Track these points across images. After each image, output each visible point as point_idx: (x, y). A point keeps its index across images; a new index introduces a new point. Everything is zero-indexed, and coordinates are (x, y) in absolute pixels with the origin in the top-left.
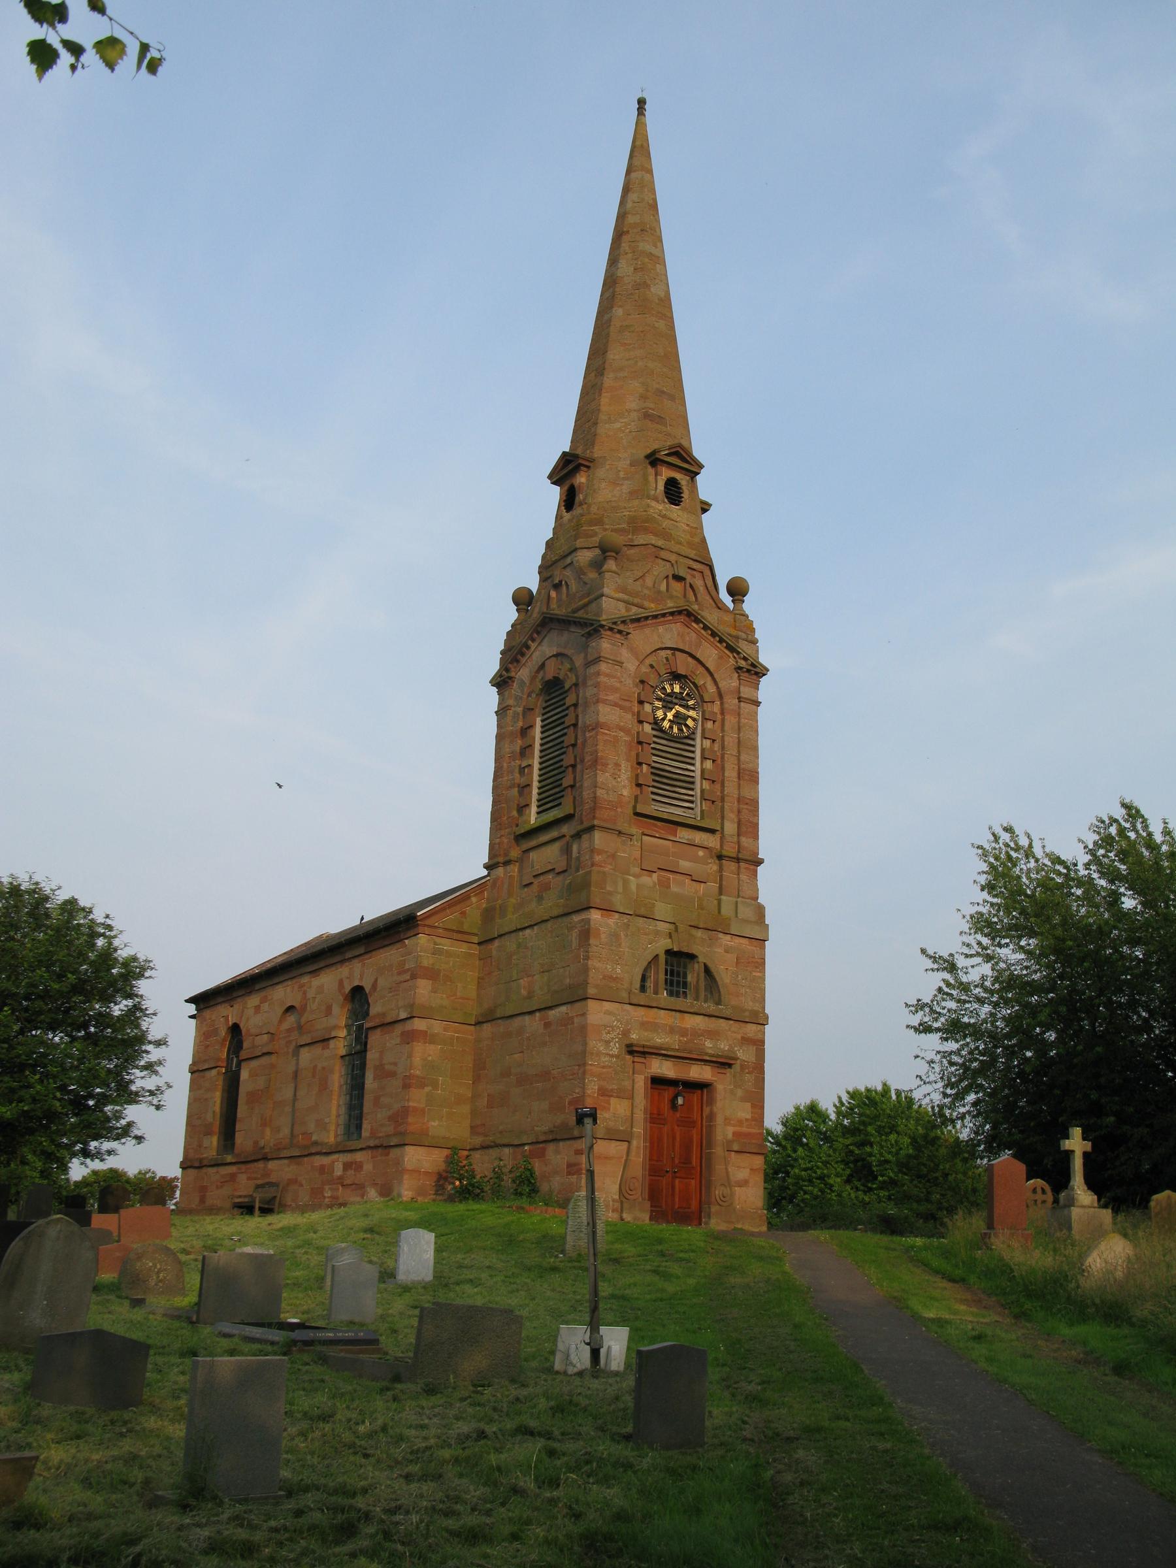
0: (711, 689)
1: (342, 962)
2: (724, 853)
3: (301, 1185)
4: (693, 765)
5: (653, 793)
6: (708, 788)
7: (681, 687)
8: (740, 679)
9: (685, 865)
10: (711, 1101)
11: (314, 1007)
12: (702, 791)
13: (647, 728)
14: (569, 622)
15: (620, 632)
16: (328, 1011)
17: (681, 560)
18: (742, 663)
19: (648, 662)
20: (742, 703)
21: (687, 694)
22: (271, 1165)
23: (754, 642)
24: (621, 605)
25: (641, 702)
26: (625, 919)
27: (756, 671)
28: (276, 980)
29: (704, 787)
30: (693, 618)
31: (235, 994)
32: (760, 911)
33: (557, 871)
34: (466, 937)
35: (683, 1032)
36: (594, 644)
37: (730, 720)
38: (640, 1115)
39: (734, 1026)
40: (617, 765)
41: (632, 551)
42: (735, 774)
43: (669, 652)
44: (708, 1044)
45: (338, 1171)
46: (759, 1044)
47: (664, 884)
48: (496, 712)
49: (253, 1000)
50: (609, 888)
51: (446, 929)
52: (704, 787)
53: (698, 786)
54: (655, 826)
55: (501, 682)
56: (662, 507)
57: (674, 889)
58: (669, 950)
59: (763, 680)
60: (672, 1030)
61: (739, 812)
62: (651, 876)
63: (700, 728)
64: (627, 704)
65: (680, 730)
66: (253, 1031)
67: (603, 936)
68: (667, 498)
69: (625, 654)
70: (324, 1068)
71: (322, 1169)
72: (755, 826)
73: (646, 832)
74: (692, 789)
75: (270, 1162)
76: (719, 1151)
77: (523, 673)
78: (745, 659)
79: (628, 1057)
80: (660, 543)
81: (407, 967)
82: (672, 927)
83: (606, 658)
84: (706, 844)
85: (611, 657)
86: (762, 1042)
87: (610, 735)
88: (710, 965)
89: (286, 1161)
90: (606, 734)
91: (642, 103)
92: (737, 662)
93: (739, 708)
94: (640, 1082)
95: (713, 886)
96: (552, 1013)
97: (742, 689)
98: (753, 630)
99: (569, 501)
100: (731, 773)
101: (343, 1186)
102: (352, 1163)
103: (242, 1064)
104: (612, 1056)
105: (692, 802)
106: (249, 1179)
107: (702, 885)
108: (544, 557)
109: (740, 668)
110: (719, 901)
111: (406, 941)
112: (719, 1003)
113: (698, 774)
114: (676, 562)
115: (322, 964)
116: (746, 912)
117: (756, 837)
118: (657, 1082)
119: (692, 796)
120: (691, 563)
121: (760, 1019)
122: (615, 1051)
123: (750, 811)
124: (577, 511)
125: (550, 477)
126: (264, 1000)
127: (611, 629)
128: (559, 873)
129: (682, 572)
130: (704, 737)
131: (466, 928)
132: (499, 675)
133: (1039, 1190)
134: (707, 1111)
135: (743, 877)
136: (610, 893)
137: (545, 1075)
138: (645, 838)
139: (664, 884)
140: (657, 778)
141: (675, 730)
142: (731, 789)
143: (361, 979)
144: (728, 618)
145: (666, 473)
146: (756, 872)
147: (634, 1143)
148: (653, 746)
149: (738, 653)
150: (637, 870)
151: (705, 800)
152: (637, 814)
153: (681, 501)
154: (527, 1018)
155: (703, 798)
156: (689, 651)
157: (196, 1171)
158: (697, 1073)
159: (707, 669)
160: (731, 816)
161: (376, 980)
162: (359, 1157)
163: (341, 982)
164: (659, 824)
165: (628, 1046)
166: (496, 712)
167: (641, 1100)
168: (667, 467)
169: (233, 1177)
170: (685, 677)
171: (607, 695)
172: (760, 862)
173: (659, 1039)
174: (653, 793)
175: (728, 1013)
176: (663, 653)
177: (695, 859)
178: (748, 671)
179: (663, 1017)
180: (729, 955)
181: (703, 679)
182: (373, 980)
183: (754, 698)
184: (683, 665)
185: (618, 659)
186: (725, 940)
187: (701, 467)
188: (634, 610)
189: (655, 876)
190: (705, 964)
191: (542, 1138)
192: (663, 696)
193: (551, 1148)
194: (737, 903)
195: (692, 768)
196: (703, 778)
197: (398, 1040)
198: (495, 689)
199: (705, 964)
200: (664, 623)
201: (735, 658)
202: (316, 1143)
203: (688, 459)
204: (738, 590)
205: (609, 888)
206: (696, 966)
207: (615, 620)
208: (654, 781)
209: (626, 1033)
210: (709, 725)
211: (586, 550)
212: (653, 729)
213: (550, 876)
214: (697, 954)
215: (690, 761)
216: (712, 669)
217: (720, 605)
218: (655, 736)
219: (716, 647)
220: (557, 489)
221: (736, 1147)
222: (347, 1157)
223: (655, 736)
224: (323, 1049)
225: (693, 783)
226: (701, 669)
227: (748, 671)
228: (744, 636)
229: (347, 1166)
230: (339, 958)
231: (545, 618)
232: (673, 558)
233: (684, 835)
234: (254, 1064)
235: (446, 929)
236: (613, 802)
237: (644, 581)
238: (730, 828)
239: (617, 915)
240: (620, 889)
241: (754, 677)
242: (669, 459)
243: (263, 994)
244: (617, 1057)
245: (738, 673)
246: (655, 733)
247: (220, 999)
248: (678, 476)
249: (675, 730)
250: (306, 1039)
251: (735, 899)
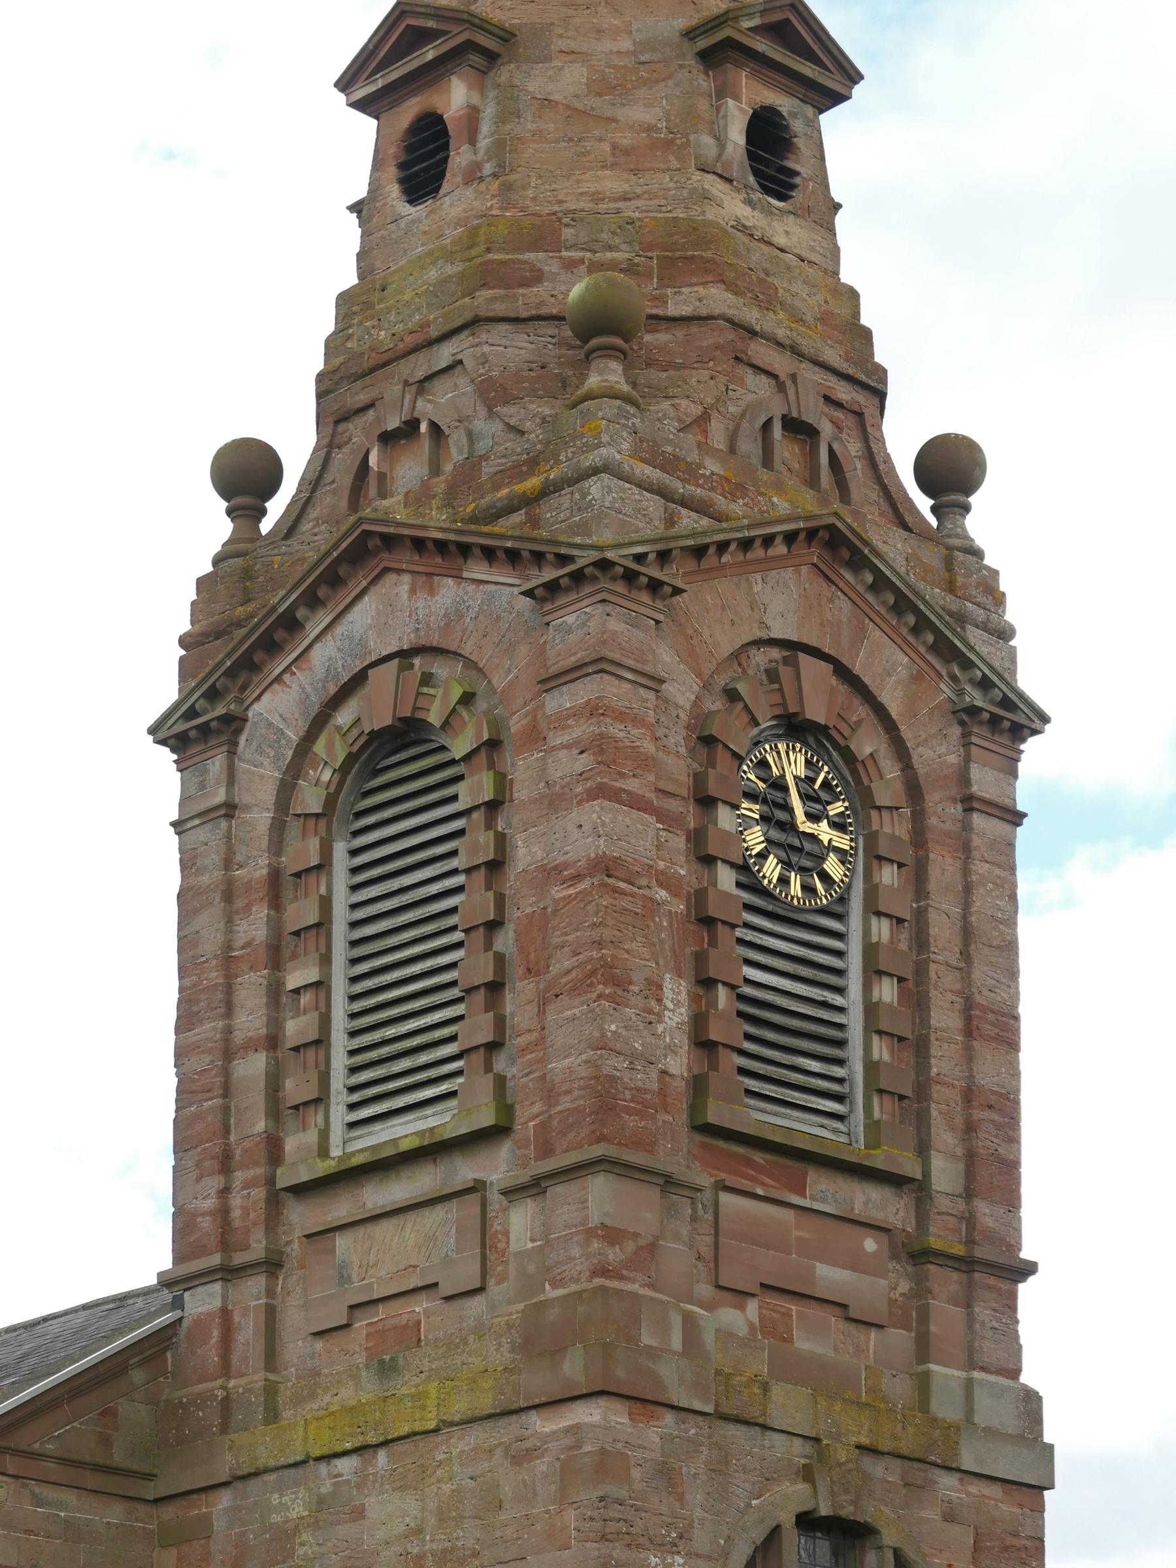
4: (840, 991)
5: (742, 1071)
6: (886, 1057)
7: (808, 763)
8: (967, 745)
12: (871, 1067)
13: (726, 878)
14: (465, 550)
15: (655, 586)
18: (975, 697)
19: (721, 681)
20: (975, 815)
21: (826, 784)
23: (1005, 633)
24: (654, 504)
25: (707, 802)
29: (876, 1056)
30: (845, 554)
32: (1031, 1403)
33: (446, 1289)
36: (570, 619)
40: (654, 987)
41: (660, 338)
43: (775, 653)
48: (174, 824)
50: (647, 1339)
51: (62, 1461)
52: (876, 1056)
53: (855, 1053)
54: (749, 1163)
58: (806, 1513)
59: (1031, 747)
62: (741, 1307)
65: (808, 889)
67: (636, 1473)
68: (757, 173)
69: (665, 658)
72: (1010, 1169)
73: (732, 1181)
74: (840, 1062)
78: (985, 684)
80: (751, 316)
83: (612, 662)
84: (877, 1216)
85: (630, 662)
87: (633, 895)
90: (623, 893)
92: (960, 693)
93: (967, 827)
97: (975, 772)
98: (999, 600)
105: (839, 1098)
107: (873, 1334)
108: (332, 346)
109: (973, 711)
113: (855, 1021)
114: (793, 377)
117: (1011, 1199)
119: (840, 1081)
120: (833, 382)
123: (998, 1126)
125: (345, 84)
127: (630, 577)
128: (448, 1299)
129: (813, 412)
130: (873, 910)
131: (118, 1458)
132: (184, 711)
135: (982, 1312)
136: (653, 1353)
138: (725, 1198)
140: (752, 1030)
141: (795, 887)
144: (932, 556)
146: (1013, 1297)
148: (740, 933)
149: (967, 665)
150: (705, 1290)
151: (880, 1091)
153: (793, 187)
155: (875, 1088)
156: (832, 652)
159: (880, 711)
160: (944, 1137)
164: (759, 1157)
166: (174, 824)
168: (754, 73)
170: (823, 730)
171: (622, 775)
172: (1027, 1270)
174: (742, 1071)
177: (857, 1262)
180: (955, 1529)
183: (1007, 801)
185: (649, 669)
186: (947, 1483)
187: (853, 76)
188: (688, 520)
192: (761, 785)
195: (838, 1000)
196: (872, 1027)
198: (166, 756)
201: (954, 678)
203: (816, 48)
205: (647, 1339)
206: (871, 1558)
207: (639, 549)
208: (748, 1037)
210: (888, 875)
211: (504, 327)
212: (739, 885)
213: (420, 1306)
214: (878, 1525)
217: (909, 519)
218: (748, 907)
219: (905, 647)
220: (367, 127)
223: (748, 907)
225: (841, 1044)
226: (861, 711)
227: (994, 722)
228: (980, 615)
231: (366, 534)
232: (781, 363)
235: (62, 1461)
236: (646, 1091)
237: (705, 432)
239: (669, 1417)
240: (677, 1343)
241: (1005, 740)
242: (761, 45)
245: (962, 723)
246: (746, 896)
248: (784, 103)
249: (795, 887)
251: (962, 1374)
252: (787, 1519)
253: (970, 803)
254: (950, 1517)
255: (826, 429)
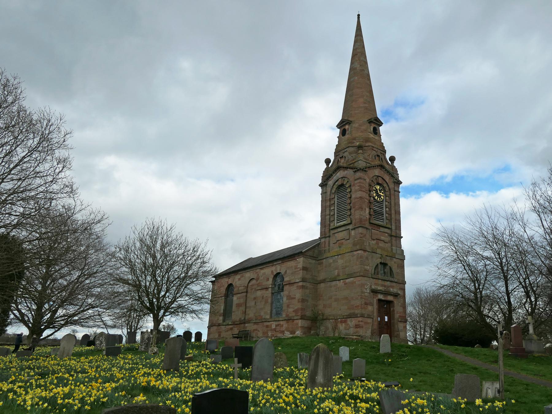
0: (387, 188)
1: (272, 266)
2: (393, 234)
3: (259, 331)
4: (383, 209)
5: (374, 217)
9: (382, 238)
10: (394, 307)
11: (262, 278)
12: (386, 217)
13: (372, 198)
15: (365, 171)
16: (268, 279)
17: (379, 150)
18: (395, 181)
22: (246, 325)
24: (365, 163)
26: (370, 253)
27: (399, 183)
28: (247, 271)
31: (230, 275)
34: (314, 258)
35: (385, 286)
37: (392, 197)
38: (375, 311)
39: (398, 285)
40: (365, 209)
42: (394, 212)
43: (376, 177)
44: (391, 290)
45: (274, 327)
46: (404, 290)
47: (377, 244)
49: (238, 277)
53: (385, 215)
55: (323, 185)
56: (372, 136)
57: (380, 245)
60: (382, 286)
61: (396, 223)
63: (385, 199)
64: (366, 191)
65: (380, 199)
66: (238, 286)
70: (266, 297)
71: (267, 326)
74: (383, 216)
75: (246, 324)
76: (396, 321)
77: (330, 183)
78: (396, 179)
79: (372, 293)
80: (374, 146)
81: (298, 267)
82: (381, 255)
84: (387, 232)
86: (405, 289)
88: (391, 266)
89: (253, 324)
91: (359, 15)
94: (375, 301)
95: (390, 244)
96: (347, 281)
99: (343, 133)
100: (393, 212)
101: (275, 331)
102: (279, 324)
103: (402, 291)
104: (368, 293)
105: (383, 220)
106: (237, 329)
108: (336, 149)
109: (395, 182)
110: (392, 249)
111: (298, 259)
112: (393, 278)
113: (384, 212)
115: (265, 266)
116: (399, 252)
118: (380, 301)
121: (404, 283)
122: (368, 292)
124: (347, 136)
125: (337, 126)
126: (242, 276)
127: (363, 170)
129: (379, 154)
130: (386, 201)
131: (315, 256)
133: (507, 334)
134: (392, 309)
137: (346, 298)
139: (377, 244)
141: (379, 199)
142: (393, 216)
143: (280, 270)
145: (373, 125)
147: (374, 318)
149: (394, 177)
150: (370, 239)
152: (370, 223)
154: (337, 281)
157: (217, 327)
158: (390, 298)
159: (386, 182)
160: (393, 224)
161: (286, 271)
162: (281, 323)
163: (272, 272)
164: (375, 226)
165: (372, 290)
167: (376, 306)
169: (231, 329)
173: (380, 288)
174: (374, 217)
175: (396, 281)
176: (375, 177)
178: (397, 183)
179: (380, 282)
181: (385, 185)
182: (285, 271)
184: (380, 181)
186: (394, 259)
188: (368, 165)
189: (375, 241)
190: (390, 266)
191: (345, 317)
193: (349, 320)
194: (396, 249)
196: (386, 213)
197: (296, 288)
198: (320, 188)
199: (390, 266)
200: (375, 168)
202: (264, 319)
204: (392, 159)
205: (365, 244)
206: (387, 267)
209: (371, 286)
210: (387, 198)
213: (343, 241)
215: (382, 208)
216: (387, 182)
221: (400, 320)
222: (277, 323)
224: (266, 291)
225: (383, 215)
229: (276, 326)
230: (271, 264)
232: (376, 150)
233: (382, 229)
234: (239, 295)
238: (393, 228)
239: (367, 252)
242: (374, 121)
243: (241, 275)
244: (369, 293)
247: (225, 277)
248: (376, 126)
249: (379, 199)
250: (259, 288)
252: (379, 263)
253: (395, 191)
254: (395, 263)
255: (380, 156)
